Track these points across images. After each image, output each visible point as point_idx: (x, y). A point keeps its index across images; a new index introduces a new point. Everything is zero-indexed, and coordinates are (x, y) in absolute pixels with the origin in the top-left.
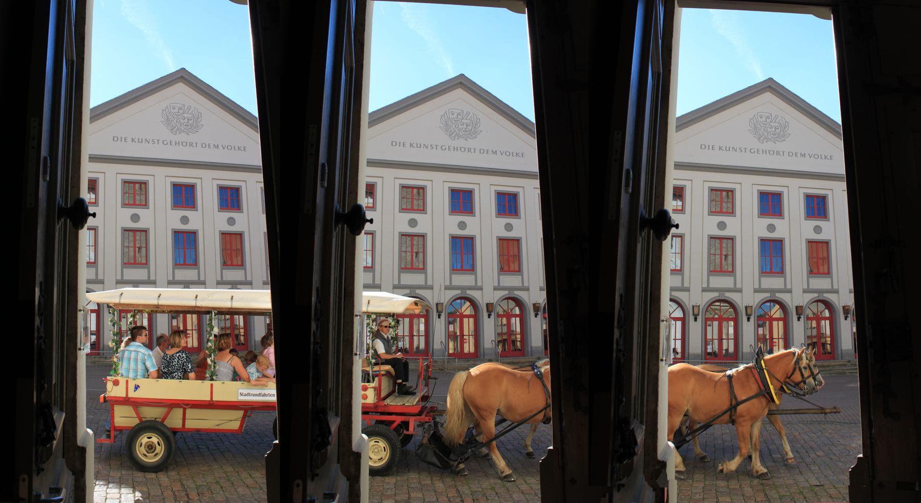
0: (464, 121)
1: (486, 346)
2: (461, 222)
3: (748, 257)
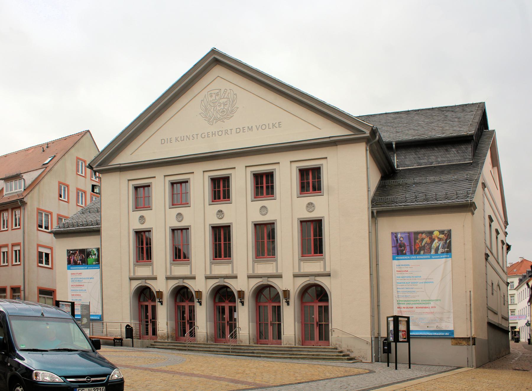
0: (222, 101)
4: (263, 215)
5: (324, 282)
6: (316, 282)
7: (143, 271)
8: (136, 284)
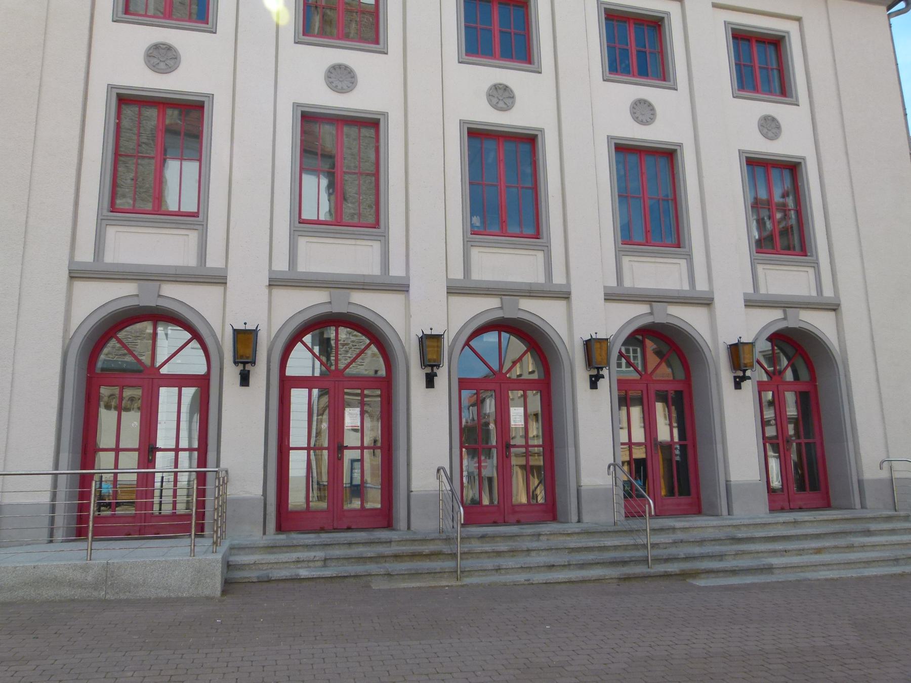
1: (416, 486)
2: (156, 47)
3: (426, 180)
4: (642, 123)
5: (820, 323)
6: (353, 310)
7: (141, 246)
8: (97, 299)
